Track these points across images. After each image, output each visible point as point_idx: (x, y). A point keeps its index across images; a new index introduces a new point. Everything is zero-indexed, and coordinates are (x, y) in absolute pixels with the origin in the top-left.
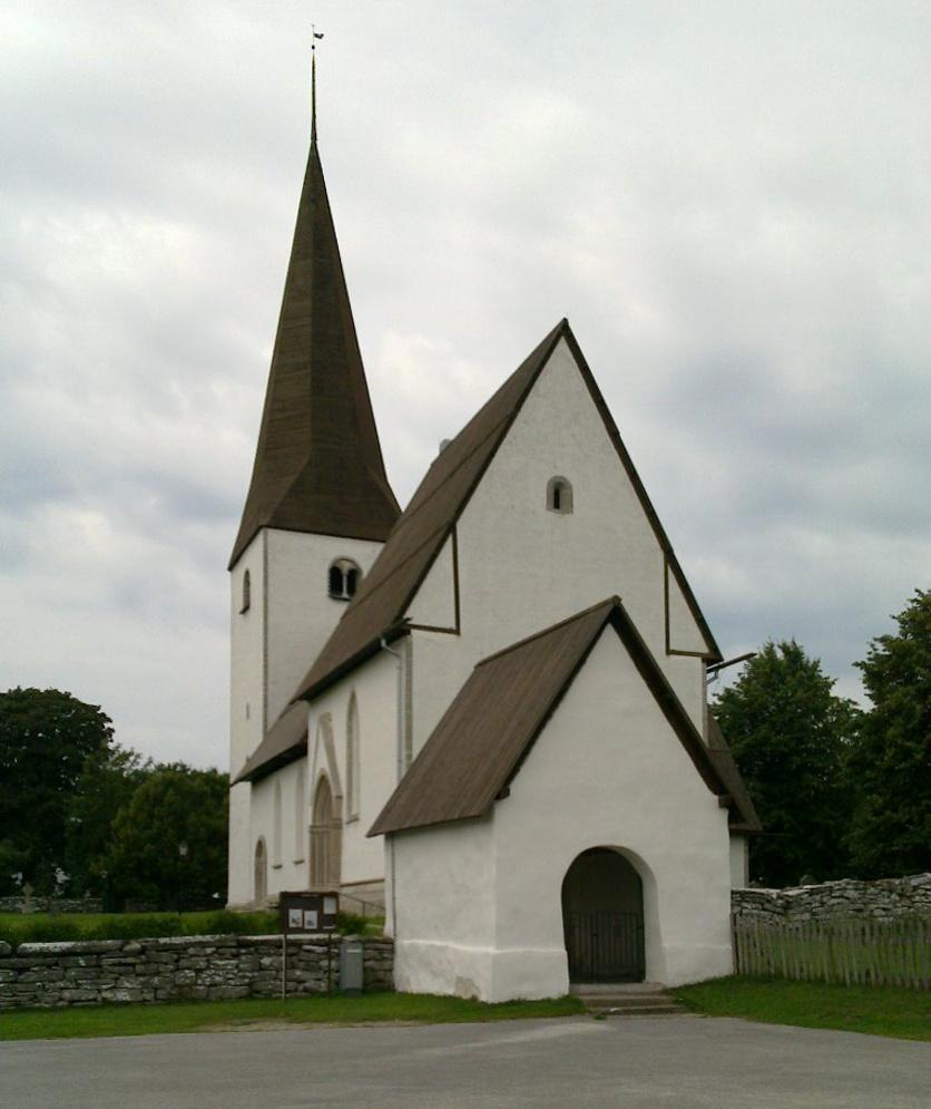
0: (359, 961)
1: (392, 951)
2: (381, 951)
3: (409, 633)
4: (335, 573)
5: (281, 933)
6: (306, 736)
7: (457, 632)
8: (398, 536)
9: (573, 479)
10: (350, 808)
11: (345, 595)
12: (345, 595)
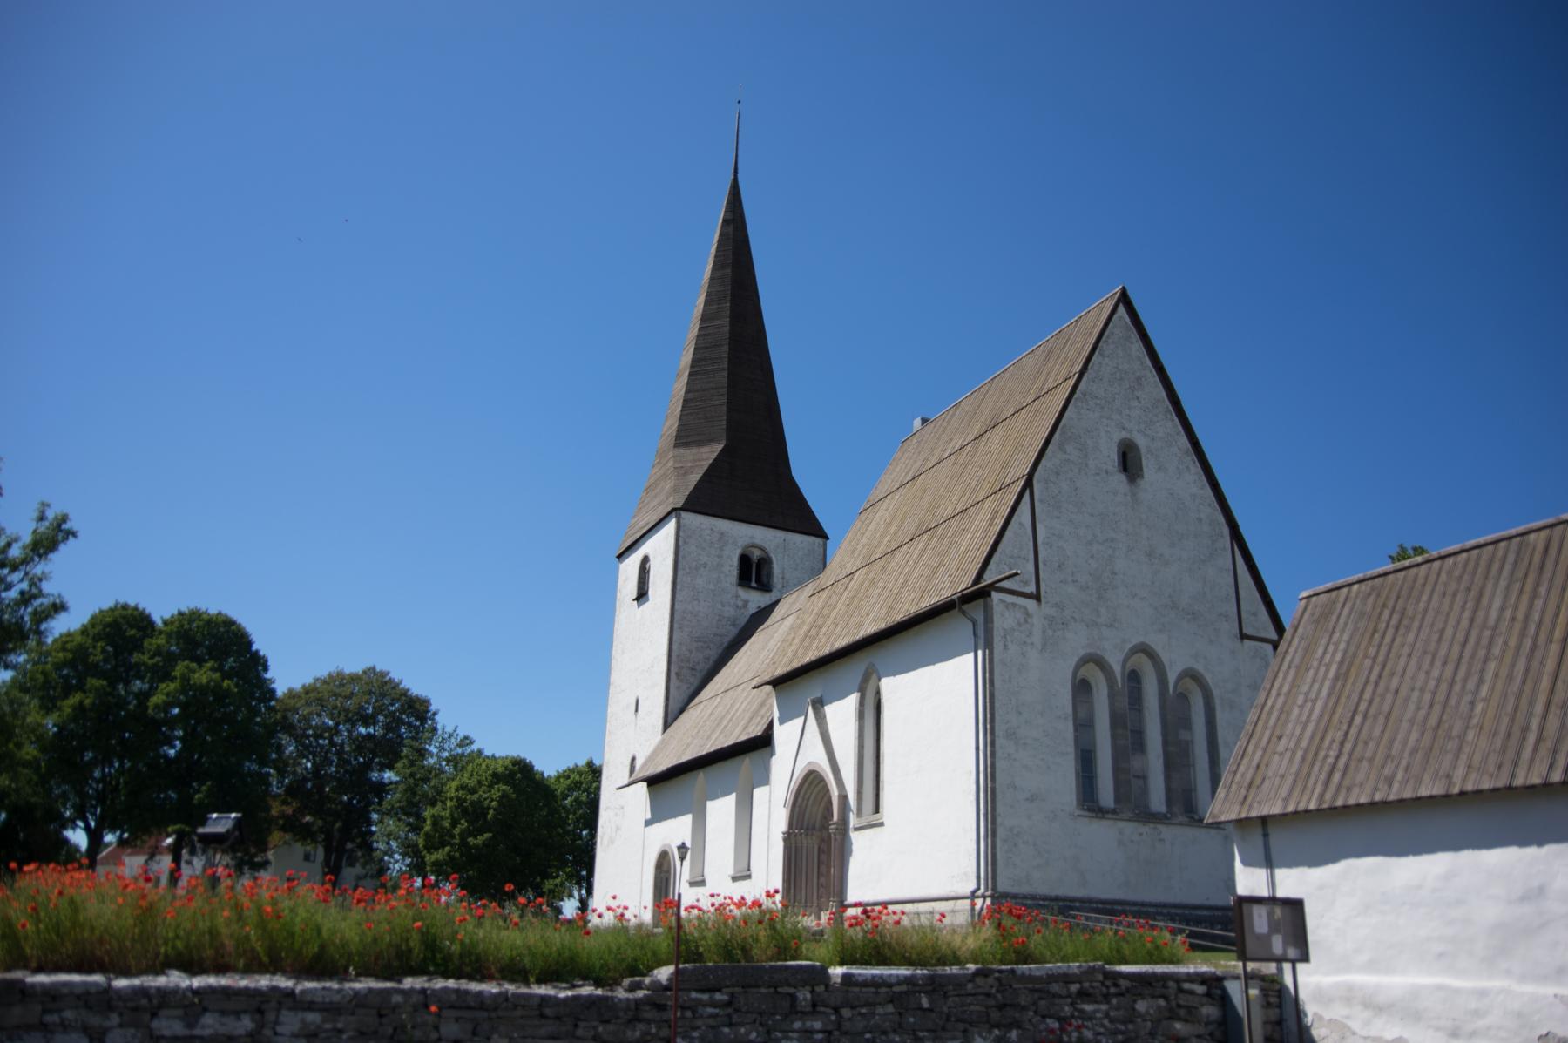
4: (745, 560)
9: (1141, 442)
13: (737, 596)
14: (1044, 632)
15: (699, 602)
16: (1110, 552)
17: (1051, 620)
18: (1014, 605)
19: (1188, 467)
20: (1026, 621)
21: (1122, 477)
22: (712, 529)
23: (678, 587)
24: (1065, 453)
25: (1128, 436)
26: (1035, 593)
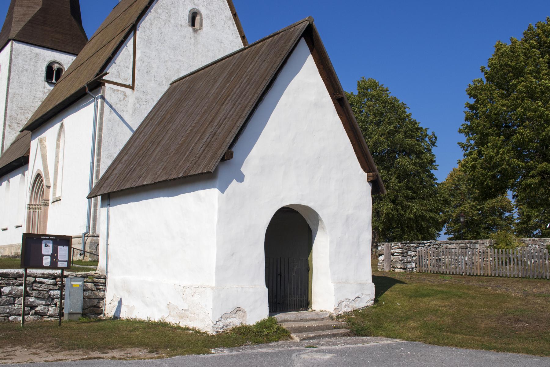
0: (81, 291)
1: (105, 284)
2: (96, 284)
3: (104, 85)
4: (49, 69)
5: (21, 267)
6: (28, 151)
7: (132, 87)
8: (87, 50)
9: (203, 11)
10: (54, 193)
11: (54, 81)
12: (54, 81)
13: (44, 87)
14: (134, 105)
15: (23, 89)
16: (178, 67)
17: (137, 99)
18: (118, 90)
19: (229, 27)
20: (124, 99)
21: (191, 29)
22: (31, 51)
23: (11, 81)
24: (158, 13)
25: (196, 7)
26: (131, 85)
